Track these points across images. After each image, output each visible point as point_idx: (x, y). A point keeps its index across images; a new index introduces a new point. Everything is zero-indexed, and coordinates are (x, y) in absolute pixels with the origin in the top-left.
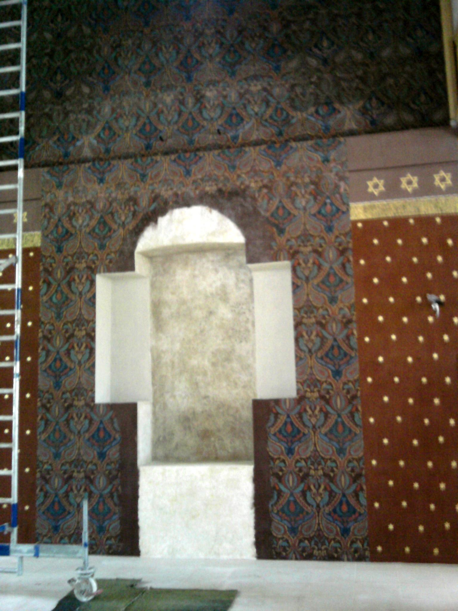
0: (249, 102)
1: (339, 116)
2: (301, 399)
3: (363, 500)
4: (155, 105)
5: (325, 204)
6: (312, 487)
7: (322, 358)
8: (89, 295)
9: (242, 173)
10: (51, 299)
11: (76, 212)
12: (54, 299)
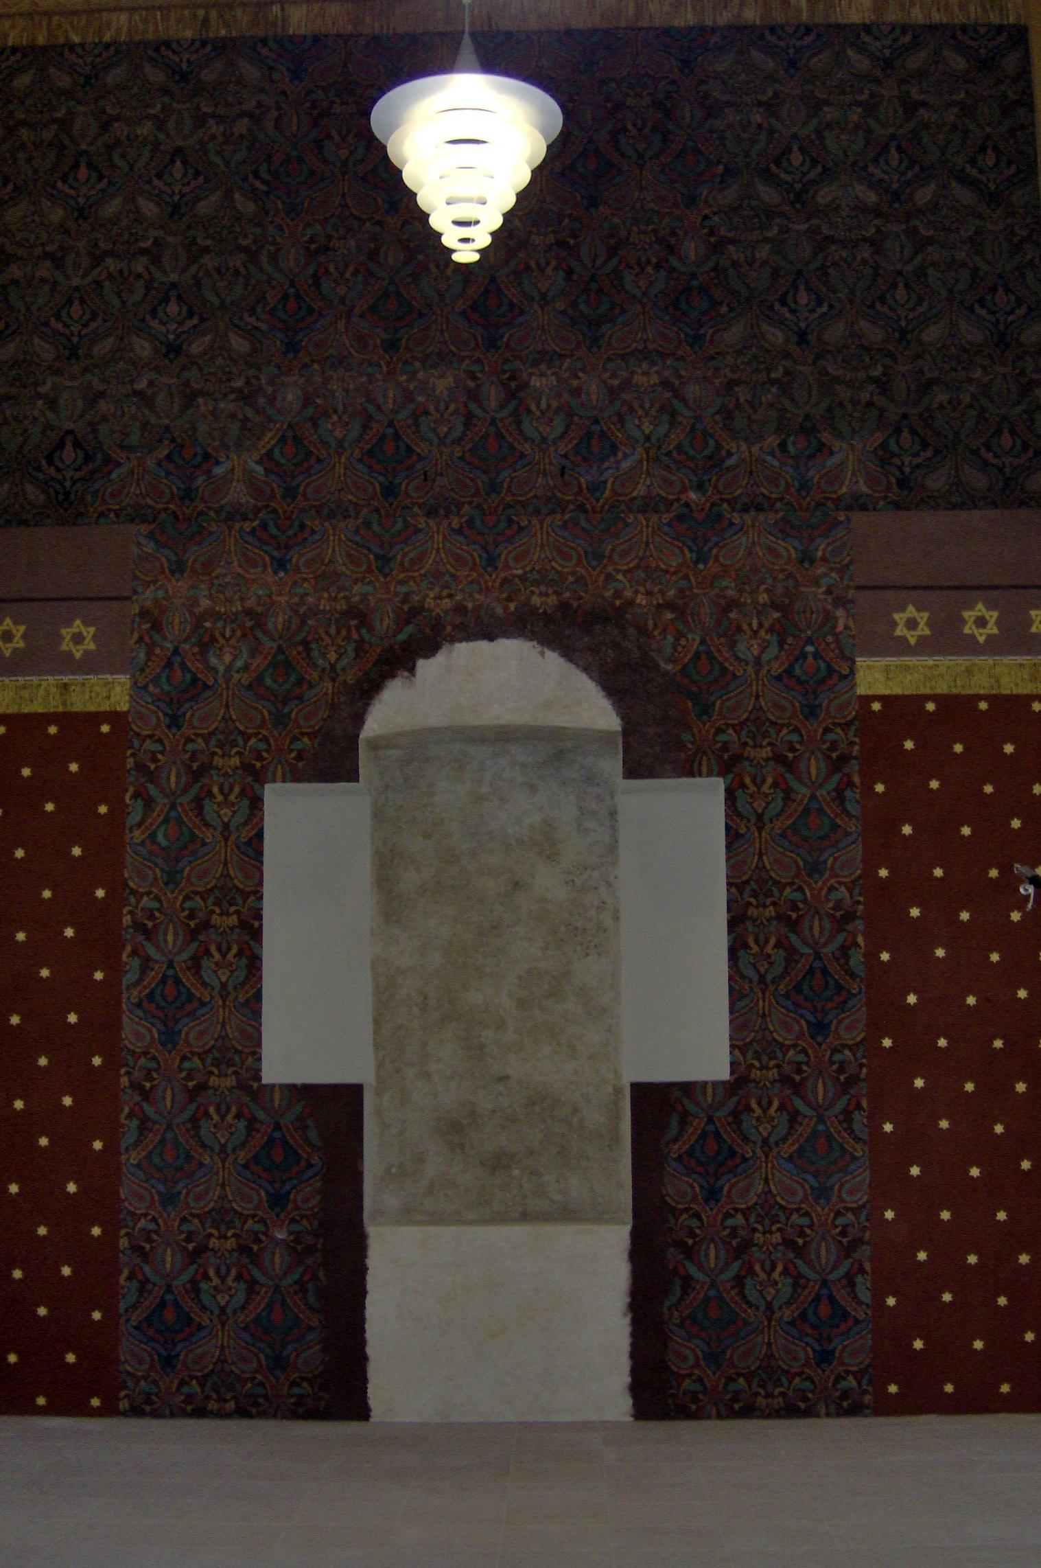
0: (632, 410)
1: (831, 462)
2: (739, 1081)
3: (865, 1296)
4: (409, 397)
5: (804, 656)
6: (757, 1268)
7: (787, 996)
8: (246, 834)
9: (617, 571)
10: (152, 837)
11: (217, 634)
12: (160, 838)
